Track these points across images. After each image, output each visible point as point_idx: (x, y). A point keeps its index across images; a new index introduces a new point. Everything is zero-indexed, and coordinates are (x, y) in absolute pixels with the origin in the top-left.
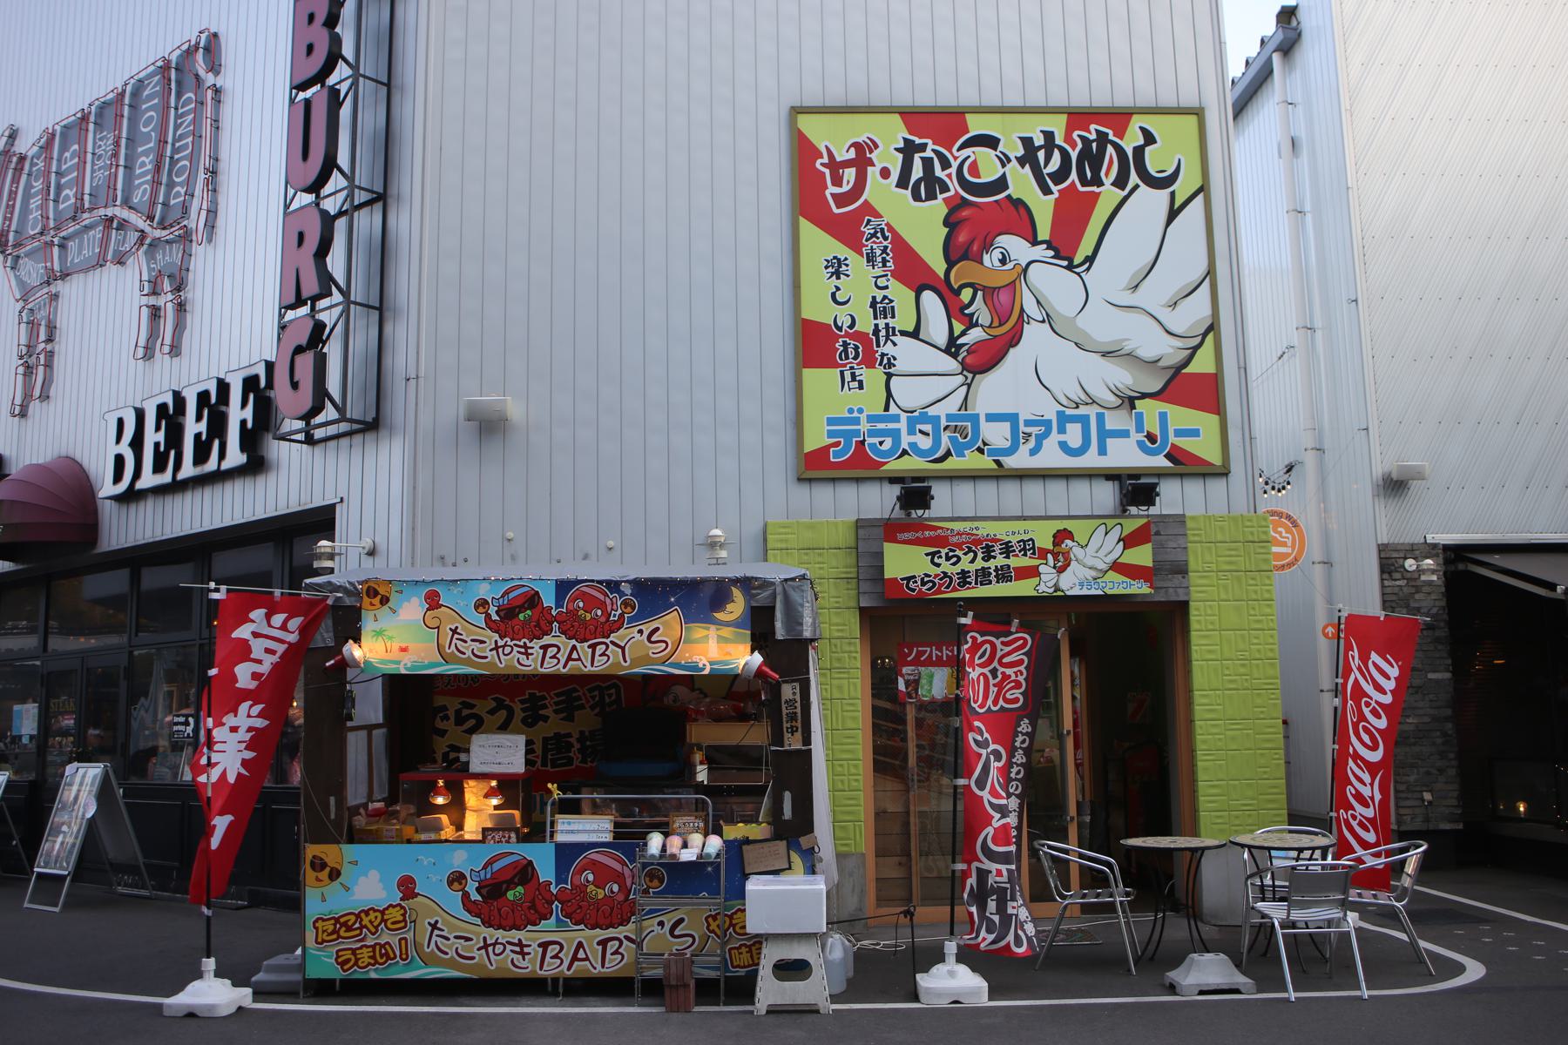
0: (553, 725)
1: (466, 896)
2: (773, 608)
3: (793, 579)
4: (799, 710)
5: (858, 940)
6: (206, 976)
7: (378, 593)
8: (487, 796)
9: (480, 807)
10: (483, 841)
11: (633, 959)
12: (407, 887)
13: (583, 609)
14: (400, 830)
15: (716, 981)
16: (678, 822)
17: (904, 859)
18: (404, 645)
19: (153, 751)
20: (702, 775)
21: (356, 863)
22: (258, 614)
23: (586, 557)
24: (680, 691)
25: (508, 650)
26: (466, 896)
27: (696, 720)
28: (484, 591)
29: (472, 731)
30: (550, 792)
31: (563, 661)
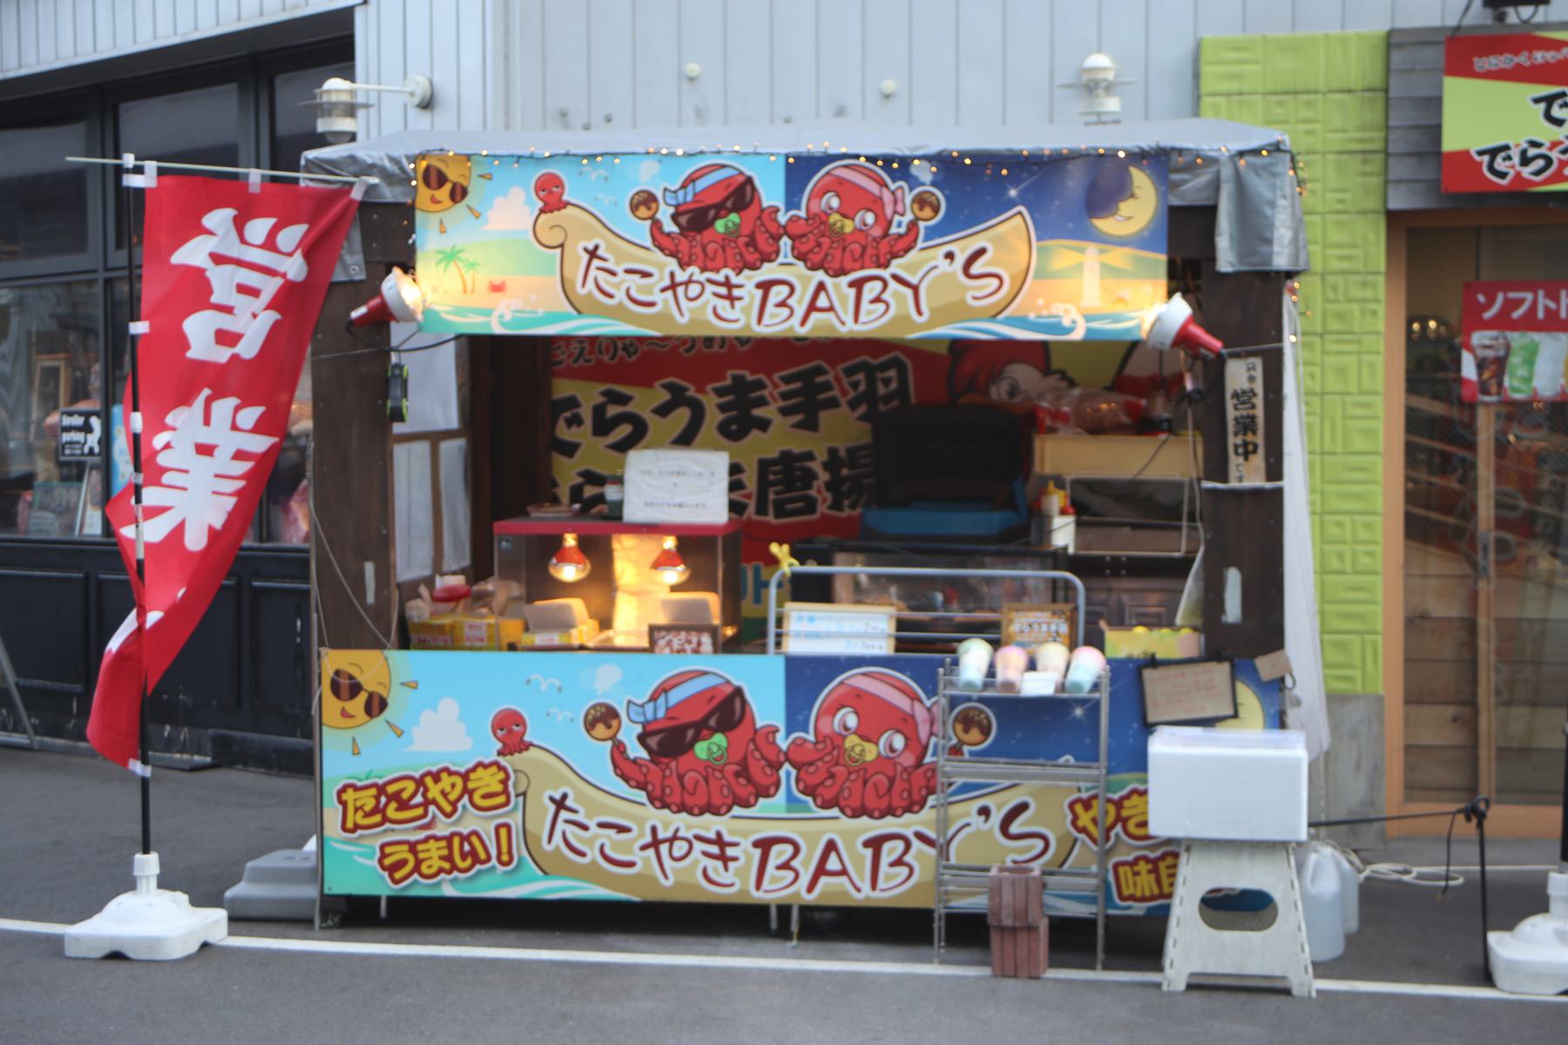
0: (780, 435)
1: (618, 749)
2: (1210, 212)
3: (1256, 152)
4: (1259, 412)
5: (1366, 862)
6: (142, 885)
7: (445, 180)
8: (658, 565)
9: (645, 586)
10: (650, 650)
11: (930, 876)
12: (511, 731)
13: (837, 211)
14: (496, 627)
15: (1087, 925)
16: (1018, 622)
17: (1466, 711)
18: (497, 280)
19: (27, 481)
20: (1063, 533)
21: (413, 685)
22: (219, 219)
23: (841, 112)
24: (1023, 374)
25: (694, 290)
26: (618, 749)
27: (1052, 430)
28: (650, 177)
29: (624, 446)
30: (774, 561)
31: (800, 312)
